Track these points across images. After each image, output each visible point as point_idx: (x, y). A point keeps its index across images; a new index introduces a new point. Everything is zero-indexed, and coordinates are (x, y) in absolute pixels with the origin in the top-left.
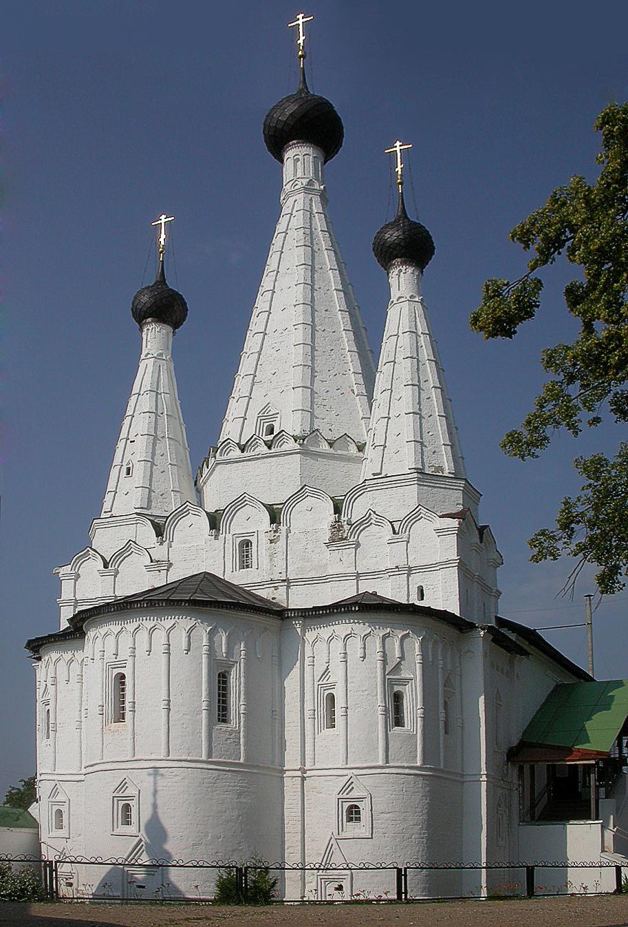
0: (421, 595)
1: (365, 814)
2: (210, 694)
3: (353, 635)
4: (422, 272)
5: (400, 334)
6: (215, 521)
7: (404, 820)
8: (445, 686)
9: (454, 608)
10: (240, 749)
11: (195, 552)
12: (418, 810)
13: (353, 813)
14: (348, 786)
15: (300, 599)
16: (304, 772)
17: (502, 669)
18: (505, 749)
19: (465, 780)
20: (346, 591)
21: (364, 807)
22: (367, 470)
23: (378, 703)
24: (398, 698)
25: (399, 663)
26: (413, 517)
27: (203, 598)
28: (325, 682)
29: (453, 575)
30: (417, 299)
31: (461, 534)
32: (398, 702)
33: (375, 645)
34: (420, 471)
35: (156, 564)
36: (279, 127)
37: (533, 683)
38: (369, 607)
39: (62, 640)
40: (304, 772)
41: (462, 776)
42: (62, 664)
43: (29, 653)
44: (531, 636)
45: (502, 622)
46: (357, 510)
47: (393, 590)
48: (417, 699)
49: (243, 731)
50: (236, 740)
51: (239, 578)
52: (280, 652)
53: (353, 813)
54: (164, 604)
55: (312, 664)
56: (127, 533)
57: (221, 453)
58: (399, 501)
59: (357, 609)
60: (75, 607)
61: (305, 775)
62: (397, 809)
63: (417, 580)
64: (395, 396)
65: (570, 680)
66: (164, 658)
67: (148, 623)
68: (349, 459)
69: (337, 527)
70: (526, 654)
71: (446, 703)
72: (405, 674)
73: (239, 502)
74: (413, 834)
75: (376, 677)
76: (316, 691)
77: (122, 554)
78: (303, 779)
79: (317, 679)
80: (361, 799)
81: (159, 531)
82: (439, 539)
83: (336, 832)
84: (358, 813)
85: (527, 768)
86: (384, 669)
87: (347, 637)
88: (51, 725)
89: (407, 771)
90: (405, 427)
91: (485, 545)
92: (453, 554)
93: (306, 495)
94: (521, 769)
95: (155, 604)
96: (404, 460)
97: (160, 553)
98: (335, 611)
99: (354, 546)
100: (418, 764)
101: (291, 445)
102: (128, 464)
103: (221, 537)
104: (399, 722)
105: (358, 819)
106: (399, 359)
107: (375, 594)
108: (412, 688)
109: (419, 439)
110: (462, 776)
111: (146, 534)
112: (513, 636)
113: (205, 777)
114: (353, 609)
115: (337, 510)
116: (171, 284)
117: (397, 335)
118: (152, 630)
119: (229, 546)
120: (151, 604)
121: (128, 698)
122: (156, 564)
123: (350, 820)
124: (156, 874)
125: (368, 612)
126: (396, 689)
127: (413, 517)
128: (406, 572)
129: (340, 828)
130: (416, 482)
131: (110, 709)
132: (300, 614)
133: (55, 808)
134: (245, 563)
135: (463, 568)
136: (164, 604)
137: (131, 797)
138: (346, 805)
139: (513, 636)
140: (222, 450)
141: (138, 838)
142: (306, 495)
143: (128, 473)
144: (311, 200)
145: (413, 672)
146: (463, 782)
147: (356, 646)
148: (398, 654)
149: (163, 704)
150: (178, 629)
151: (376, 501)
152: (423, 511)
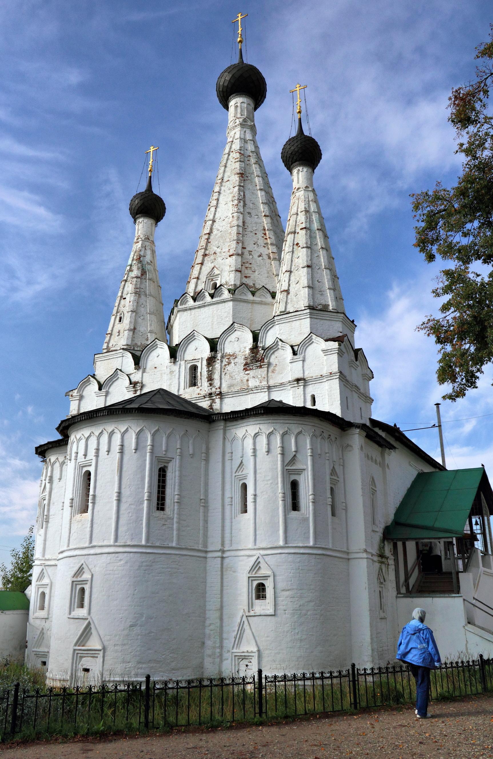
0: (314, 403)
1: (269, 592)
5: (299, 213)
6: (174, 353)
7: (301, 597)
8: (331, 474)
9: (336, 410)
10: (173, 534)
11: (162, 374)
12: (312, 587)
13: (260, 591)
14: (256, 566)
15: (229, 405)
16: (223, 551)
17: (376, 460)
18: (380, 529)
19: (350, 557)
20: (260, 398)
21: (269, 585)
22: (278, 308)
23: (279, 490)
24: (294, 486)
25: (295, 456)
26: (307, 341)
27: (152, 408)
29: (335, 384)
30: (310, 189)
31: (340, 353)
33: (277, 441)
34: (311, 308)
36: (226, 84)
37: (401, 472)
38: (272, 410)
39: (57, 447)
40: (223, 551)
41: (348, 553)
42: (57, 465)
43: (38, 459)
44: (394, 431)
45: (375, 423)
46: (269, 340)
47: (292, 398)
48: (308, 486)
49: (177, 518)
50: (170, 526)
51: (189, 394)
52: (208, 449)
53: (260, 591)
54: (120, 412)
56: (116, 363)
57: (181, 303)
58: (299, 329)
59: (262, 412)
61: (224, 555)
62: (295, 587)
63: (311, 390)
64: (295, 255)
65: (427, 469)
66: (118, 455)
67: (110, 427)
68: (266, 304)
69: (255, 349)
70: (392, 447)
71: (332, 489)
72: (298, 466)
73: (190, 338)
74: (308, 611)
75: (277, 468)
76: (233, 482)
77: (113, 377)
78: (223, 558)
79: (234, 471)
80: (266, 577)
81: (137, 361)
82: (325, 357)
83: (246, 610)
84: (264, 590)
85: (400, 544)
86: (283, 461)
87: (256, 435)
88: (45, 517)
89: (302, 551)
90: (302, 276)
91: (360, 363)
92: (335, 368)
94: (395, 546)
95: (113, 412)
96: (301, 298)
97: (136, 377)
98: (247, 414)
99: (266, 366)
100: (311, 544)
101: (226, 295)
103: (178, 363)
104: (295, 507)
105: (264, 597)
107: (281, 402)
108: (305, 477)
109: (311, 285)
110: (348, 553)
112: (383, 434)
113: (143, 560)
114: (260, 412)
115: (256, 338)
116: (156, 191)
117: (297, 214)
118: (111, 434)
119: (183, 368)
120: (111, 412)
121: (91, 492)
123: (258, 597)
124: (99, 656)
126: (293, 477)
127: (307, 341)
129: (251, 606)
131: (77, 502)
132: (222, 417)
133: (41, 590)
134: (193, 383)
135: (343, 377)
136: (120, 412)
137: (85, 581)
138: (255, 583)
139: (383, 434)
140: (181, 301)
141: (87, 622)
143: (120, 321)
144: (245, 132)
145: (306, 463)
146: (349, 559)
147: (263, 440)
148: (293, 449)
149: (115, 497)
151: (281, 331)
152: (314, 337)
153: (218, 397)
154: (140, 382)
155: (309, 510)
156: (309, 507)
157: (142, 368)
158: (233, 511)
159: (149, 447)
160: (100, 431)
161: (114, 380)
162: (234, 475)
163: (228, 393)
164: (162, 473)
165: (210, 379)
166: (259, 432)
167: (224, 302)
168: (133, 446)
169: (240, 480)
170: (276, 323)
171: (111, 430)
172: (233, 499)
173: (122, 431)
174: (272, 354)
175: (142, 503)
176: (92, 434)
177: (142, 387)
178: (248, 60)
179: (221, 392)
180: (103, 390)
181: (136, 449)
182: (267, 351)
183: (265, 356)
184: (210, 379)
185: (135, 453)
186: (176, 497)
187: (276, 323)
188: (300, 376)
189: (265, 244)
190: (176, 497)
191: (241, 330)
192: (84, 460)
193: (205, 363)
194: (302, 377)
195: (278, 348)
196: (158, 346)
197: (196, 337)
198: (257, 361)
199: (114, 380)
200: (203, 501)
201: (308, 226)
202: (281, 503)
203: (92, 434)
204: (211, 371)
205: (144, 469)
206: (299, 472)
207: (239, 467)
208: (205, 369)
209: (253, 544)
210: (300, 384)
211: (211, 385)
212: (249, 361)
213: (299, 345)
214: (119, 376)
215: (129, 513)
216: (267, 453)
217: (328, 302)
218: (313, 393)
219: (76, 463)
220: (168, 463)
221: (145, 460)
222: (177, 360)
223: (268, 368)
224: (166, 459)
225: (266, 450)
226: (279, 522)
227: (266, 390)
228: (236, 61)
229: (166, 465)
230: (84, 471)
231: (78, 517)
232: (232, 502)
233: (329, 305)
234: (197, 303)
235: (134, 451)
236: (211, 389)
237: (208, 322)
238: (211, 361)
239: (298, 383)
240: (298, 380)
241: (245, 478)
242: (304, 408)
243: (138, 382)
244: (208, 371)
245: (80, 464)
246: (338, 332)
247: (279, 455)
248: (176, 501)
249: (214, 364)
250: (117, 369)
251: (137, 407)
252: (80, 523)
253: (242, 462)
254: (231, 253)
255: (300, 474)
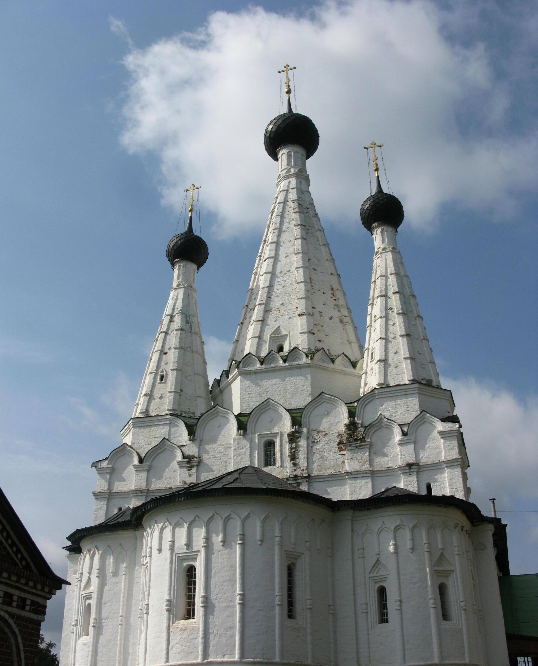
2: (281, 588)
3: (402, 527)
4: (396, 231)
25: (442, 554)
26: (420, 420)
28: (375, 574)
32: (188, 588)
35: (189, 462)
55: (362, 556)
57: (243, 365)
60: (147, 496)
63: (426, 478)
69: (352, 426)
79: (368, 571)
81: (191, 431)
93: (323, 401)
97: (192, 450)
99: (368, 446)
102: (162, 372)
106: (390, 293)
111: (181, 434)
115: (352, 414)
116: (197, 232)
122: (189, 462)
125: (368, 509)
128: (416, 470)
130: (417, 391)
140: (244, 362)
142: (323, 401)
144: (301, 182)
145: (457, 564)
150: (252, 518)
153: (305, 480)
154: (196, 455)
155: (461, 619)
156: (461, 616)
157: (198, 439)
158: (369, 620)
159: (277, 539)
160: (210, 515)
161: (159, 451)
162: (368, 576)
163: (318, 477)
164: (290, 572)
165: (293, 457)
166: (400, 525)
167: (300, 368)
168: (258, 536)
169: (375, 583)
170: (377, 397)
171: (226, 515)
172: (369, 606)
173: (243, 517)
174: (373, 433)
175: (273, 608)
176: (197, 518)
177: (199, 463)
178: (299, 109)
179: (309, 475)
180: (144, 463)
181: (262, 541)
182: (369, 429)
183: (366, 435)
184: (293, 457)
185: (261, 545)
186: (309, 602)
187: (377, 397)
188: (412, 460)
189: (335, 305)
190: (309, 602)
191: (331, 402)
192: (185, 551)
193: (286, 438)
194: (415, 461)
195: (382, 426)
196: (220, 414)
197: (270, 407)
198: (356, 440)
199: (159, 451)
200: (332, 607)
201: (401, 291)
202: (432, 611)
203: (197, 518)
204: (294, 448)
205: (273, 566)
206: (447, 573)
207: (373, 567)
208: (287, 447)
209: (403, 661)
210: (412, 470)
211: (295, 465)
212: (344, 439)
213: (409, 424)
214: (166, 447)
215: (257, 621)
216: (412, 551)
217: (431, 377)
218: (429, 481)
219: (172, 554)
220: (296, 559)
221: (273, 555)
222: (248, 432)
223: (370, 449)
224: (295, 554)
225: (411, 547)
226: (431, 634)
227: (370, 475)
228: (284, 110)
229: (294, 561)
230: (185, 564)
231: (183, 623)
232: (367, 609)
233: (432, 381)
234: (263, 367)
235: (221, 544)
236: (295, 470)
237: (279, 389)
238: (293, 438)
239: (410, 468)
240: (410, 465)
241: (384, 579)
242: (452, 498)
243: (193, 457)
244: (291, 449)
245: (177, 555)
246: (447, 411)
247: (426, 554)
248: (308, 607)
249: (298, 440)
250: (164, 438)
251: (221, 487)
252: (186, 632)
253: (378, 560)
254: (300, 312)
255: (447, 577)
